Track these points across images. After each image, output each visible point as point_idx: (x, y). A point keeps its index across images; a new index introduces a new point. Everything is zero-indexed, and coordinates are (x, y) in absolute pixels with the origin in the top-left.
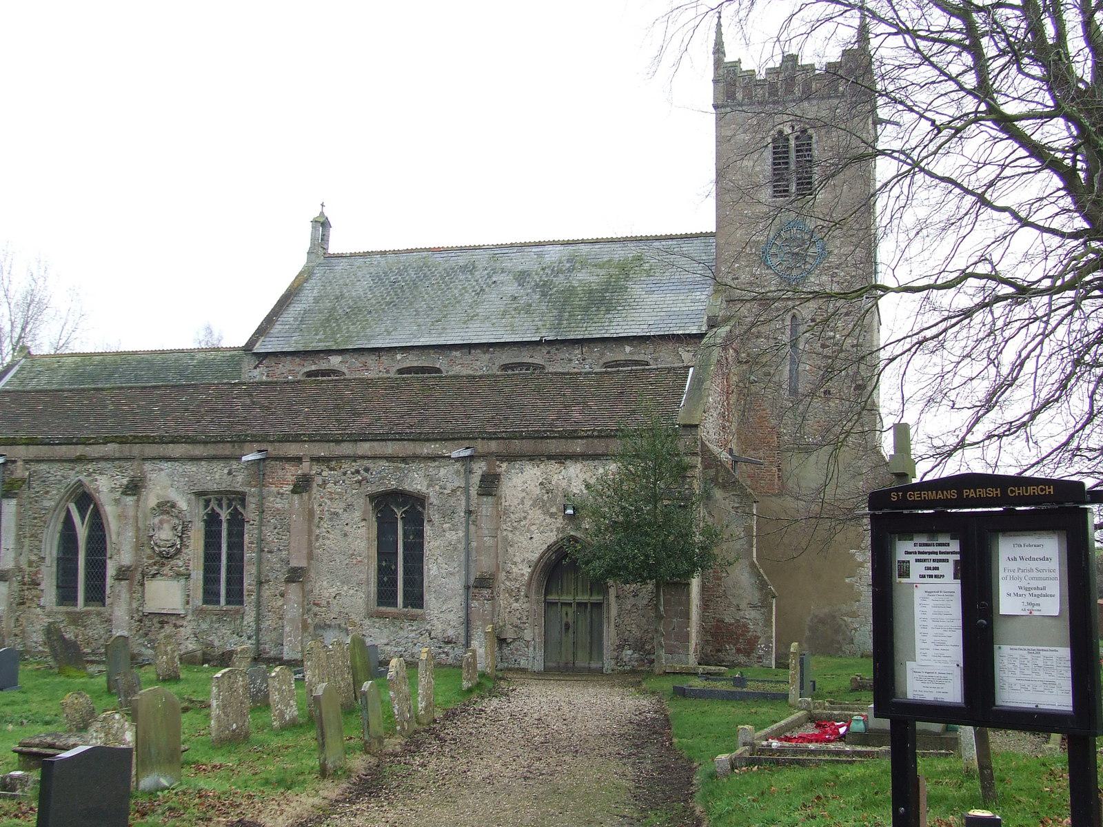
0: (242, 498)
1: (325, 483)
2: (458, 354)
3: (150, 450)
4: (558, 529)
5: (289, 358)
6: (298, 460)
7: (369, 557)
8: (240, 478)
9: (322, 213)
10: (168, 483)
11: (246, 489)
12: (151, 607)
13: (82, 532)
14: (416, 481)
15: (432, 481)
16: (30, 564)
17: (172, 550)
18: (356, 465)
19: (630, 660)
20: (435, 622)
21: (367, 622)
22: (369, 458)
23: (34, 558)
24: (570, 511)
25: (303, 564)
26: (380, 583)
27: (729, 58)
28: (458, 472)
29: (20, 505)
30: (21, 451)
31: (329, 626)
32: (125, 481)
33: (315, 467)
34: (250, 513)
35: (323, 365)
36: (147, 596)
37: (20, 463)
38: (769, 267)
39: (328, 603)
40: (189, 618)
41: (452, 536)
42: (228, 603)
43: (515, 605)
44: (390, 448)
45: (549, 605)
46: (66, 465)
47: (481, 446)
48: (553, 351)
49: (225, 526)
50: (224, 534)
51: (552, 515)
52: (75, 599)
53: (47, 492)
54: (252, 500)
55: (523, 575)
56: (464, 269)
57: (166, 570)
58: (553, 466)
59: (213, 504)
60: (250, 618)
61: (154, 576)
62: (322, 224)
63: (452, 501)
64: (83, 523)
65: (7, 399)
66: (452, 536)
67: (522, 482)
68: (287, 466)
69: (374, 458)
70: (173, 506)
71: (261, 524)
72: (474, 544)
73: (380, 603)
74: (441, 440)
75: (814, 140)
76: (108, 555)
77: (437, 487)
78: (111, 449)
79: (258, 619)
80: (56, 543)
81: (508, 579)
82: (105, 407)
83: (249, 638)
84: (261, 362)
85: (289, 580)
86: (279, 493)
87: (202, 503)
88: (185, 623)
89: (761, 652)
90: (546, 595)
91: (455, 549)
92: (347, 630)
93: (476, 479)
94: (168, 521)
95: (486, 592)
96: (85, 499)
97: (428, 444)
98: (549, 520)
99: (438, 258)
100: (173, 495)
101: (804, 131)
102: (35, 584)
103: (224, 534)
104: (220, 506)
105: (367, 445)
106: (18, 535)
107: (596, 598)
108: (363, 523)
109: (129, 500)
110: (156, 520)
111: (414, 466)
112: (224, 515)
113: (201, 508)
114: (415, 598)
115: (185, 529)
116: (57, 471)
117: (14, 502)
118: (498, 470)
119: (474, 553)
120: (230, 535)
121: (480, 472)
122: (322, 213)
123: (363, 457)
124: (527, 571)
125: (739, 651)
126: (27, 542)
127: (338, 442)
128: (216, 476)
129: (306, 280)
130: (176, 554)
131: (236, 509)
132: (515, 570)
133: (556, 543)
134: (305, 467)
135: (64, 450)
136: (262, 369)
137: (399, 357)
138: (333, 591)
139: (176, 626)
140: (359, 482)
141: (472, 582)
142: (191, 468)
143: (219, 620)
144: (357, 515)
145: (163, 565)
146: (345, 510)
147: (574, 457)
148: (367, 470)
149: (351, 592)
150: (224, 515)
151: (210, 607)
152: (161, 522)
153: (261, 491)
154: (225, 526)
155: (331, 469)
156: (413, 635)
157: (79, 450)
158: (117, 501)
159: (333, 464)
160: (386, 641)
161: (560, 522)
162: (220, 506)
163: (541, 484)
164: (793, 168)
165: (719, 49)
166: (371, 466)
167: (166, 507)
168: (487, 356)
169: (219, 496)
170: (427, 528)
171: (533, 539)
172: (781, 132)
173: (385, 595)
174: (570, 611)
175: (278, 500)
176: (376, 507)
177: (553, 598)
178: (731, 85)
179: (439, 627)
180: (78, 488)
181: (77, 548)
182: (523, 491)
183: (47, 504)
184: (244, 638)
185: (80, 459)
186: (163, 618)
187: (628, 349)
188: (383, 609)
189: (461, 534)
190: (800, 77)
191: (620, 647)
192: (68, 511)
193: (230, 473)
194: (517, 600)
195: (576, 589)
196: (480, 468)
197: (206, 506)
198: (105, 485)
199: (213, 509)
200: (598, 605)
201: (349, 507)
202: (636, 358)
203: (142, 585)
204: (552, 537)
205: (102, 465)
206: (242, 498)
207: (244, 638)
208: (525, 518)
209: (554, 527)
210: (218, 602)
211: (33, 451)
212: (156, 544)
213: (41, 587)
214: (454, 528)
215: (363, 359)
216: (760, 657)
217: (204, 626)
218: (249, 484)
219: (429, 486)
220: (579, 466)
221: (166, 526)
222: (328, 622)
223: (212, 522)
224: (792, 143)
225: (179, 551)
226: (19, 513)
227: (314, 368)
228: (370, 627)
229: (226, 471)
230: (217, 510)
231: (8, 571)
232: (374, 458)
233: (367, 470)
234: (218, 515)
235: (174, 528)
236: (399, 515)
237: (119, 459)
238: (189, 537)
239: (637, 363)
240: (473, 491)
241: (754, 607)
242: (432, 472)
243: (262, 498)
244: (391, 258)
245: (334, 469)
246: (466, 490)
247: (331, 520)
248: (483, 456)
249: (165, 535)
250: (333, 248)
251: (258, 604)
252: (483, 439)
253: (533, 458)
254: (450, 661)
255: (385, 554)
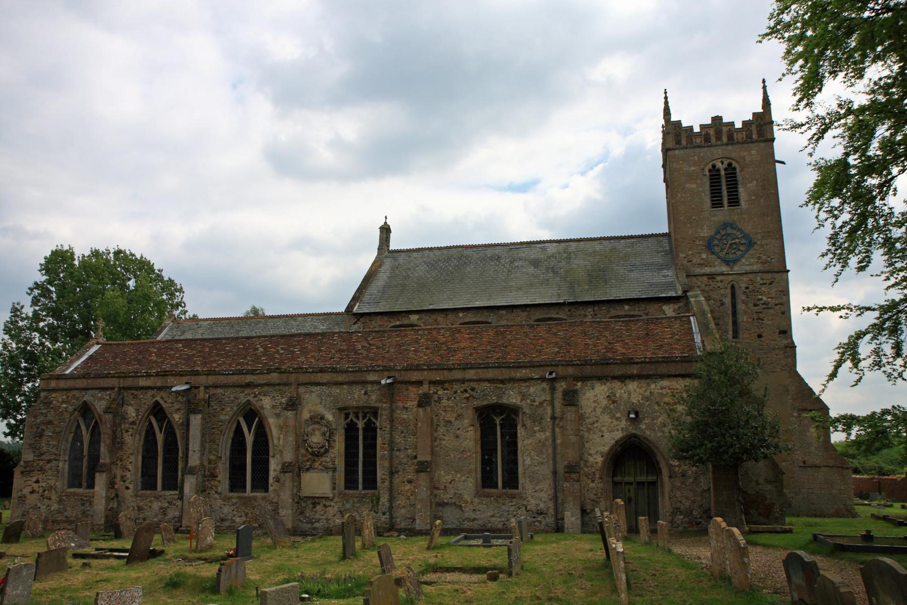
0: (375, 412)
1: (440, 399)
2: (504, 312)
3: (303, 378)
4: (622, 429)
5: (380, 317)
6: (420, 383)
7: (476, 453)
8: (374, 397)
9: (386, 223)
10: (314, 402)
11: (379, 405)
12: (306, 492)
13: (249, 439)
14: (512, 397)
15: (524, 397)
16: (210, 462)
17: (322, 450)
18: (464, 386)
19: (682, 523)
20: (530, 498)
21: (476, 500)
22: (474, 381)
23: (212, 457)
24: (632, 416)
25: (428, 458)
26: (483, 471)
27: (674, 118)
28: (544, 390)
29: (203, 418)
30: (202, 380)
31: (447, 504)
32: (283, 400)
33: (432, 388)
34: (382, 422)
35: (406, 322)
36: (303, 485)
37: (202, 388)
38: (713, 253)
39: (445, 487)
40: (336, 499)
41: (541, 436)
42: (364, 488)
43: (592, 485)
44: (491, 374)
45: (616, 484)
46: (238, 390)
47: (561, 371)
48: (573, 309)
49: (361, 432)
50: (361, 438)
51: (618, 419)
52: (245, 487)
53: (223, 409)
54: (384, 413)
55: (597, 463)
56: (492, 258)
57: (317, 465)
58: (617, 384)
59: (351, 416)
60: (384, 499)
61: (308, 470)
62: (385, 230)
63: (540, 411)
64: (250, 432)
65: (180, 345)
66: (541, 436)
67: (594, 396)
68: (410, 388)
69: (479, 380)
70: (322, 418)
71: (392, 430)
72: (559, 441)
73: (484, 487)
74: (531, 367)
75: (738, 171)
76: (271, 454)
77: (529, 401)
78: (274, 377)
79: (391, 499)
80: (229, 446)
81: (586, 466)
82: (257, 349)
83: (384, 514)
84: (358, 320)
85: (418, 471)
86: (404, 407)
87: (343, 416)
88: (333, 504)
89: (777, 515)
90: (613, 477)
91: (544, 445)
92: (461, 506)
93: (559, 395)
94: (319, 429)
95: (574, 476)
96: (251, 414)
97: (520, 370)
98: (615, 423)
99: (470, 252)
100: (321, 410)
101: (730, 165)
102: (214, 476)
103: (361, 438)
104: (357, 417)
105: (473, 372)
106: (202, 440)
107: (651, 478)
108: (471, 428)
109: (290, 414)
110: (310, 429)
111: (509, 386)
112: (361, 425)
113: (343, 419)
114: (512, 480)
115: (332, 434)
116: (230, 394)
117: (199, 416)
118: (576, 388)
119: (559, 448)
120: (365, 438)
121: (561, 389)
122: (386, 223)
123: (470, 380)
124: (600, 459)
125: (760, 514)
126: (207, 445)
127: (450, 369)
128: (356, 396)
129: (380, 266)
130: (325, 453)
131: (370, 420)
132: (591, 459)
133: (621, 439)
134: (425, 388)
135: (235, 379)
136: (359, 324)
137: (461, 315)
138: (449, 478)
139: (325, 506)
140: (467, 398)
141: (561, 469)
142: (336, 390)
143: (359, 502)
144: (466, 422)
145: (315, 461)
146: (456, 419)
147: (632, 377)
148: (473, 389)
149: (463, 478)
150: (361, 425)
151: (351, 492)
152: (313, 430)
153: (391, 407)
154: (361, 432)
155: (445, 389)
156: (512, 508)
157: (249, 378)
158: (278, 416)
159: (446, 385)
160: (491, 514)
161: (624, 423)
162: (357, 417)
163: (608, 397)
164: (724, 186)
165: (667, 112)
166: (476, 386)
167: (317, 419)
168: (525, 314)
169: (356, 411)
170: (520, 431)
171: (605, 437)
172: (714, 166)
173: (488, 480)
174: (632, 488)
175: (404, 412)
176: (479, 416)
177: (618, 479)
178: (675, 135)
179: (533, 502)
180: (154, 407)
181: (245, 450)
182: (594, 402)
183: (222, 417)
184: (380, 514)
185: (249, 385)
186: (315, 501)
187: (626, 307)
188: (487, 490)
189: (548, 434)
190: (725, 129)
191: (674, 514)
192: (239, 423)
193: (366, 393)
194: (593, 481)
195: (636, 472)
196: (561, 386)
197: (346, 418)
198: (266, 403)
199: (352, 420)
200: (653, 484)
201: (459, 417)
202: (632, 313)
203: (299, 476)
204: (619, 435)
205: (266, 389)
206: (375, 412)
207: (380, 514)
208: (597, 421)
209: (619, 428)
210: (357, 488)
211: (211, 380)
212: (310, 446)
213: (219, 478)
214: (543, 430)
215: (434, 317)
216: (776, 518)
217: (348, 506)
218: (381, 401)
219: (522, 400)
220: (636, 383)
221: (317, 432)
222: (446, 501)
223: (351, 429)
224: (723, 173)
225: (327, 451)
226: (202, 425)
227: (398, 323)
228: (479, 503)
229: (363, 392)
230: (355, 420)
231: (195, 467)
232: (479, 380)
233: (473, 389)
234: (356, 424)
235: (324, 434)
236: (498, 423)
237: (279, 384)
238: (334, 441)
239: (633, 316)
240: (558, 404)
241: (769, 482)
242: (524, 390)
243: (392, 411)
244: (438, 253)
245: (447, 389)
246: (552, 403)
247: (445, 426)
248: (564, 378)
249: (316, 439)
250: (392, 247)
251: (391, 490)
252: (563, 365)
253: (600, 378)
254: (542, 527)
255: (487, 450)
